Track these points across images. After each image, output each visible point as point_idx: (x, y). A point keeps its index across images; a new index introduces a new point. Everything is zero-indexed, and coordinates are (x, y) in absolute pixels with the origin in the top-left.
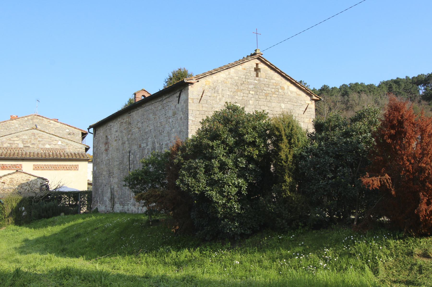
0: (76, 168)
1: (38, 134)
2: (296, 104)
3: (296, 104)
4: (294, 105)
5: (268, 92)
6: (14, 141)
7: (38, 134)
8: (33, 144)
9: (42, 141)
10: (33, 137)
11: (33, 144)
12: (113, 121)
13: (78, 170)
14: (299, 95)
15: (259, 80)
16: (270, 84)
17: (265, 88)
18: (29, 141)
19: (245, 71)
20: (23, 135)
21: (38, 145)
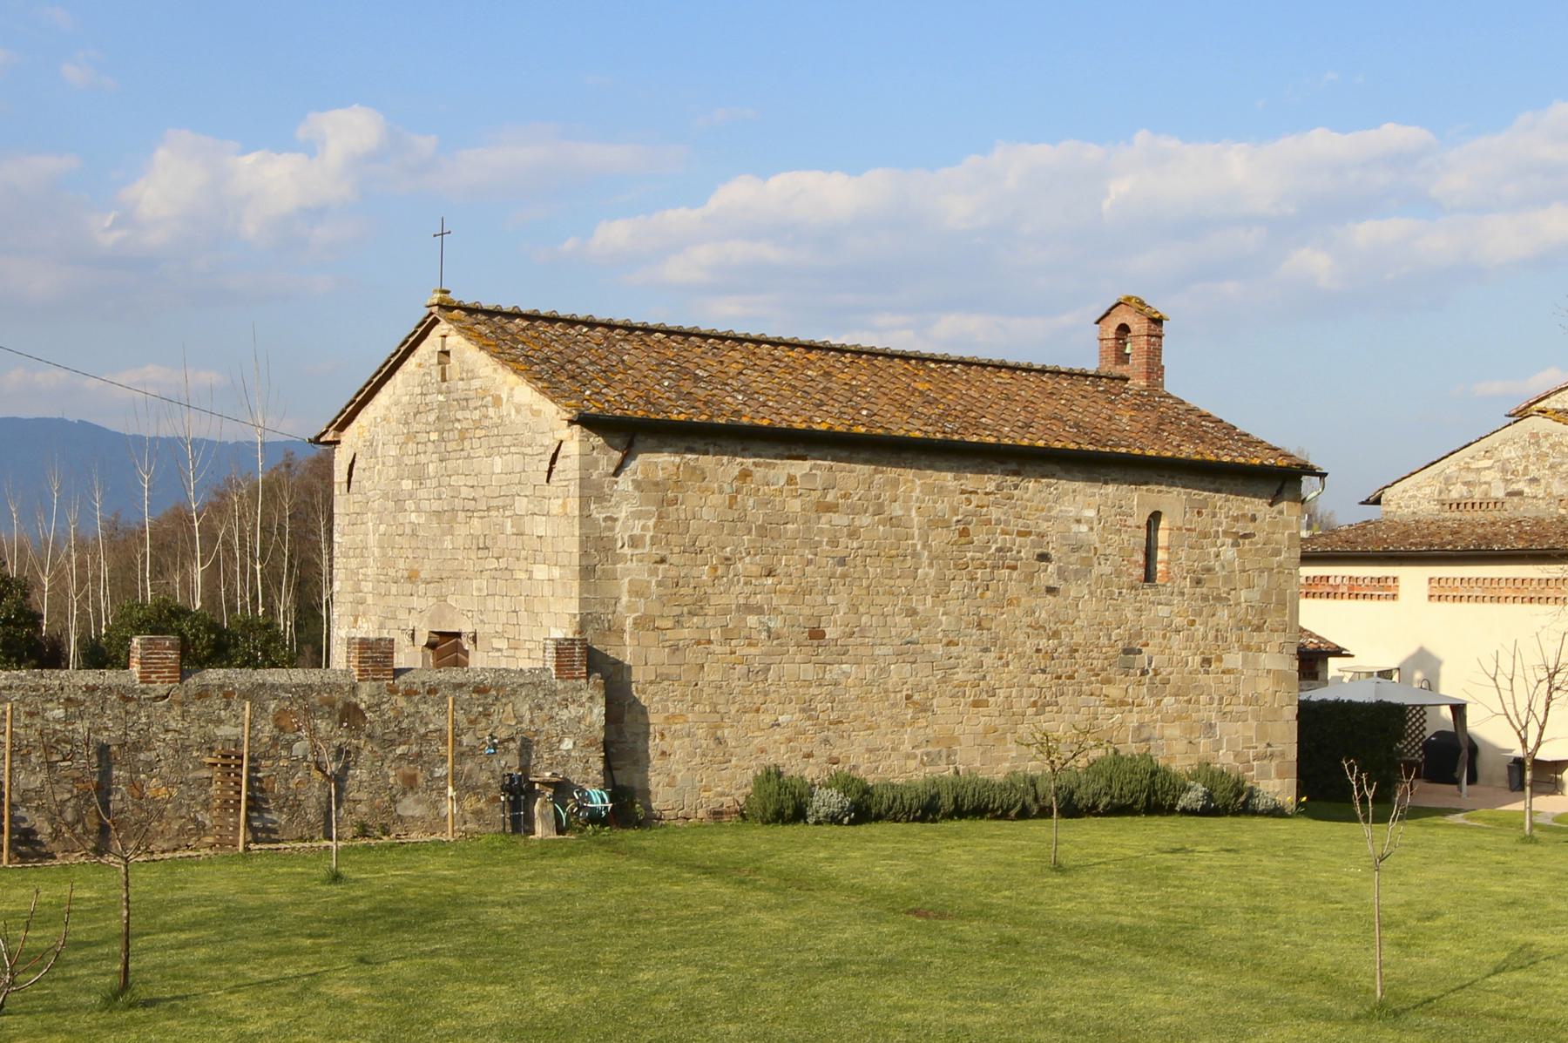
0: (1387, 591)
1: (1547, 436)
2: (529, 450)
3: (529, 450)
4: (524, 455)
5: (465, 425)
6: (1478, 470)
7: (1547, 436)
8: (1534, 480)
9: (1561, 464)
10: (1532, 450)
11: (1534, 480)
12: (966, 469)
13: (1394, 597)
14: (536, 413)
15: (449, 392)
16: (472, 394)
17: (459, 415)
18: (1520, 468)
19: (422, 371)
20: (1504, 443)
21: (1548, 485)
